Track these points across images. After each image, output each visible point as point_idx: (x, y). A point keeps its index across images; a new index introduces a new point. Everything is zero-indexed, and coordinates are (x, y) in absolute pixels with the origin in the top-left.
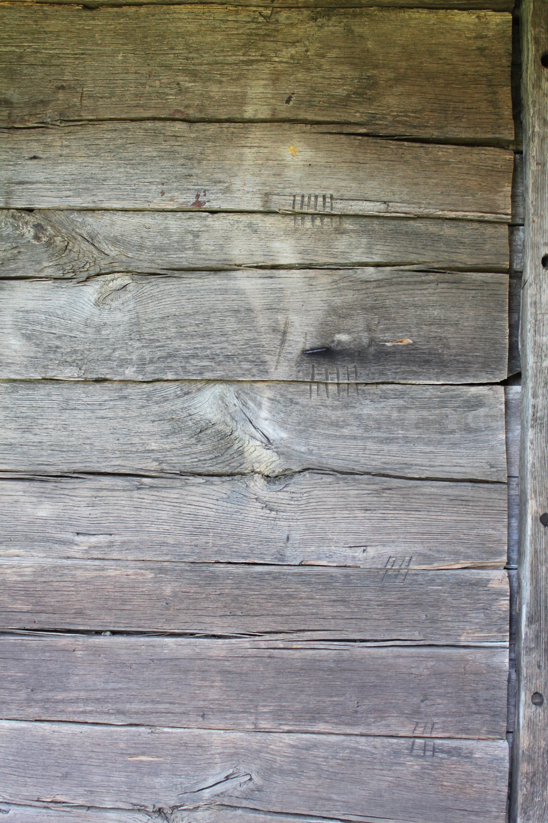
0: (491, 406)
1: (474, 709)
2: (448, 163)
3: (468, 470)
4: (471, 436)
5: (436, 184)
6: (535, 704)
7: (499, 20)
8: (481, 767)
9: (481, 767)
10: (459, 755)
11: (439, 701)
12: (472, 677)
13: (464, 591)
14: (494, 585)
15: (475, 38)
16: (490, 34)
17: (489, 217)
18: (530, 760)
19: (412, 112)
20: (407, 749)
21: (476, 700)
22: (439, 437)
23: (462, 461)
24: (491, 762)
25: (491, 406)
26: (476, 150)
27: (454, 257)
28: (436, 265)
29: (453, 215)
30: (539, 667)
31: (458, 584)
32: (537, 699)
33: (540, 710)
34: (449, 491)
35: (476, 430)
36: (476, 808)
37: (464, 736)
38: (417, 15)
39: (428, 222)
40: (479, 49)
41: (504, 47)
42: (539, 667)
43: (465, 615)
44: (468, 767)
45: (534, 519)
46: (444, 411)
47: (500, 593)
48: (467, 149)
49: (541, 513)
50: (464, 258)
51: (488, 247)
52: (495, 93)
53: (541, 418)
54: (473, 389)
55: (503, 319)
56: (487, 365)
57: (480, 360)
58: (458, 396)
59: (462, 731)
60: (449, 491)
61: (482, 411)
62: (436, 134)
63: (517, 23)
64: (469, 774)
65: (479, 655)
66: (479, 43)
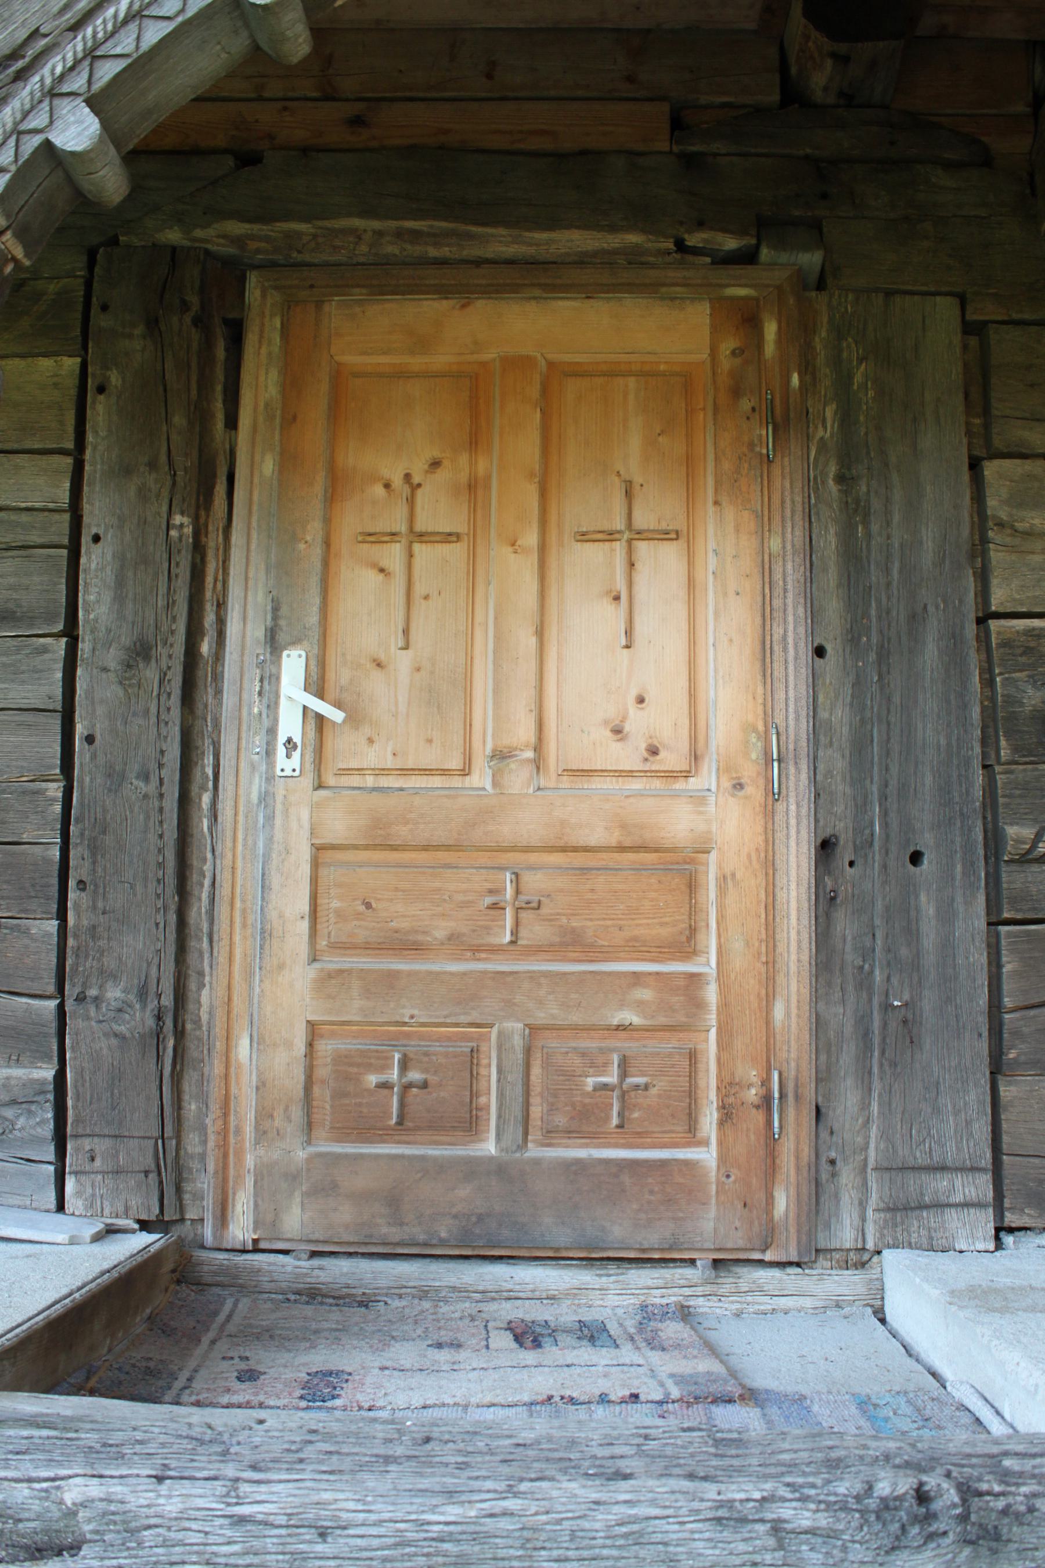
0: (54, 652)
1: (33, 894)
2: (24, 467)
3: (33, 701)
4: (36, 676)
5: (14, 484)
6: (80, 889)
7: (71, 363)
8: (36, 941)
9: (36, 941)
10: (19, 931)
11: (5, 887)
12: (31, 867)
13: (27, 798)
14: (50, 794)
15: (52, 376)
16: (63, 373)
17: (51, 505)
18: (76, 936)
19: (961, 786)
20: (895, 1204)
21: (33, 886)
22: (13, 677)
23: (30, 695)
24: (43, 937)
25: (54, 652)
26: (45, 457)
27: (27, 538)
28: (14, 544)
29: (23, 505)
30: (83, 859)
31: (23, 792)
32: (81, 884)
33: (83, 894)
34: (17, 718)
35: (41, 671)
36: (32, 975)
37: (23, 916)
38: (11, 362)
39: (11, 513)
40: (54, 384)
41: (73, 383)
42: (83, 859)
43: (27, 817)
44: (27, 941)
45: (81, 739)
46: (19, 657)
47: (54, 799)
48: (39, 457)
49: (86, 734)
50: (35, 538)
51: (53, 529)
52: (62, 415)
53: (87, 659)
54: (42, 640)
55: (61, 584)
56: (51, 619)
57: (43, 615)
58: (29, 645)
59: (21, 911)
60: (17, 718)
61: (47, 656)
62: (16, 446)
63: (84, 366)
64: (26, 947)
65: (37, 849)
66: (55, 379)
